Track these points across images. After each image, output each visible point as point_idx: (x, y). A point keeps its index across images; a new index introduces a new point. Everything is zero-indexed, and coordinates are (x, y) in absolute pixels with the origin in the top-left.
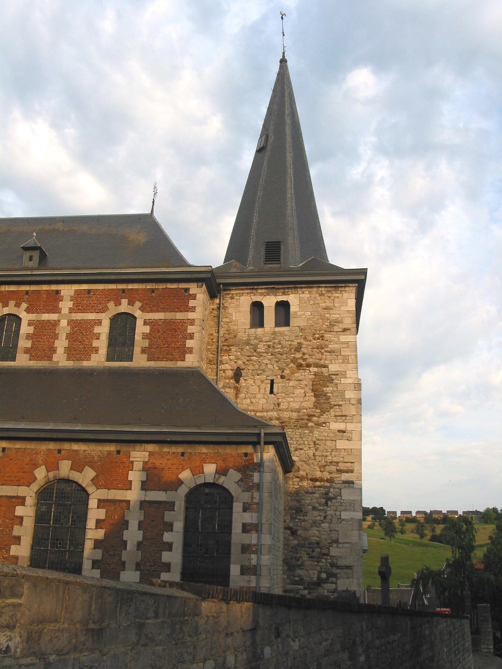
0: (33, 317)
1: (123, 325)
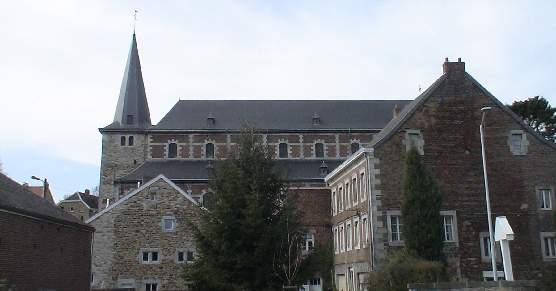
0: (181, 144)
1: (319, 147)
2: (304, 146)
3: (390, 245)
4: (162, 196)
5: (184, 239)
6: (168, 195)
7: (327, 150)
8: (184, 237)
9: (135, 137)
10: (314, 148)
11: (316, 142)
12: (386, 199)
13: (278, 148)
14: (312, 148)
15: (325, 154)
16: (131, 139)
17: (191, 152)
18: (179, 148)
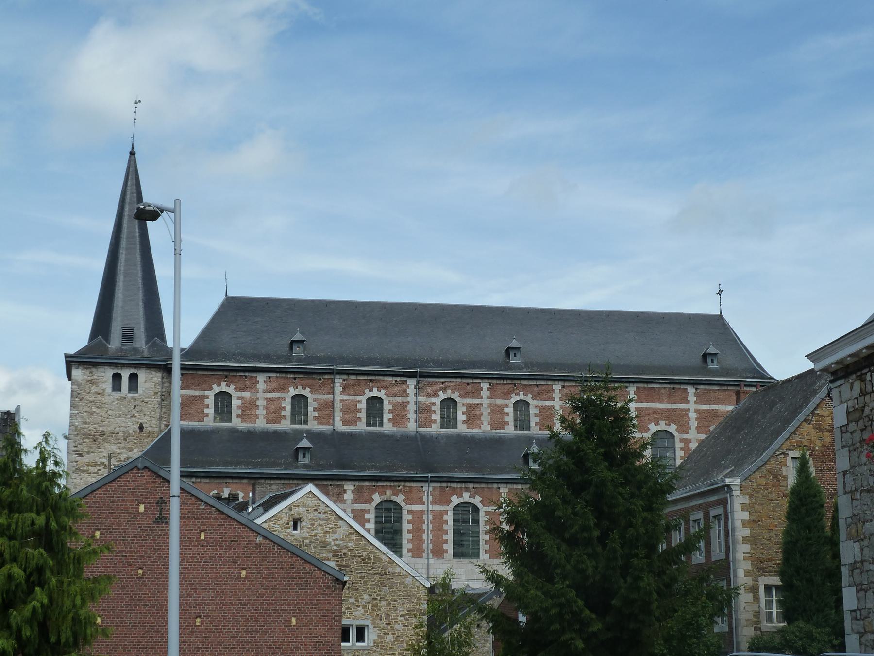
0: (240, 394)
2: (490, 405)
3: (763, 629)
4: (313, 524)
5: (352, 604)
6: (322, 523)
7: (536, 415)
8: (352, 600)
9: (142, 375)
10: (510, 410)
11: (515, 398)
12: (759, 558)
13: (437, 408)
14: (506, 410)
15: (532, 424)
16: (133, 378)
17: (261, 412)
18: (235, 403)
